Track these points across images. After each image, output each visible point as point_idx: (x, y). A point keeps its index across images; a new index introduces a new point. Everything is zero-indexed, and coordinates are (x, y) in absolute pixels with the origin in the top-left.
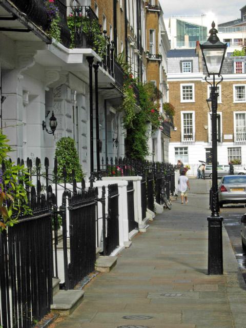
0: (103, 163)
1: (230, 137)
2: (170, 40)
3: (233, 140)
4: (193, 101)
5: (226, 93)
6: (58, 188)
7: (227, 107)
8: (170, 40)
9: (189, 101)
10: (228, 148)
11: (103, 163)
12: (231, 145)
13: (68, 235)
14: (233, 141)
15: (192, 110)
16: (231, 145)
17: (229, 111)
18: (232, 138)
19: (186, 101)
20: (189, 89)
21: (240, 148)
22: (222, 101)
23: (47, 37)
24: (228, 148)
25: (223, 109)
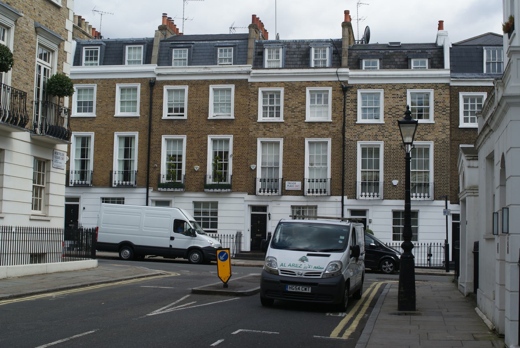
0: (7, 231)
1: (297, 185)
2: (268, 33)
3: (301, 193)
4: (93, 114)
5: (291, 103)
6: (345, 203)
7: (293, 128)
8: (268, 33)
9: (275, 119)
10: (293, 207)
11: (7, 231)
12: (298, 201)
13: (174, 303)
14: (303, 195)
15: (91, 131)
16: (298, 201)
17: (297, 137)
18: (300, 188)
19: (268, 119)
20: (469, 117)
21: (316, 207)
22: (285, 118)
23: (45, 24)
24: (293, 207)
25: (286, 132)
